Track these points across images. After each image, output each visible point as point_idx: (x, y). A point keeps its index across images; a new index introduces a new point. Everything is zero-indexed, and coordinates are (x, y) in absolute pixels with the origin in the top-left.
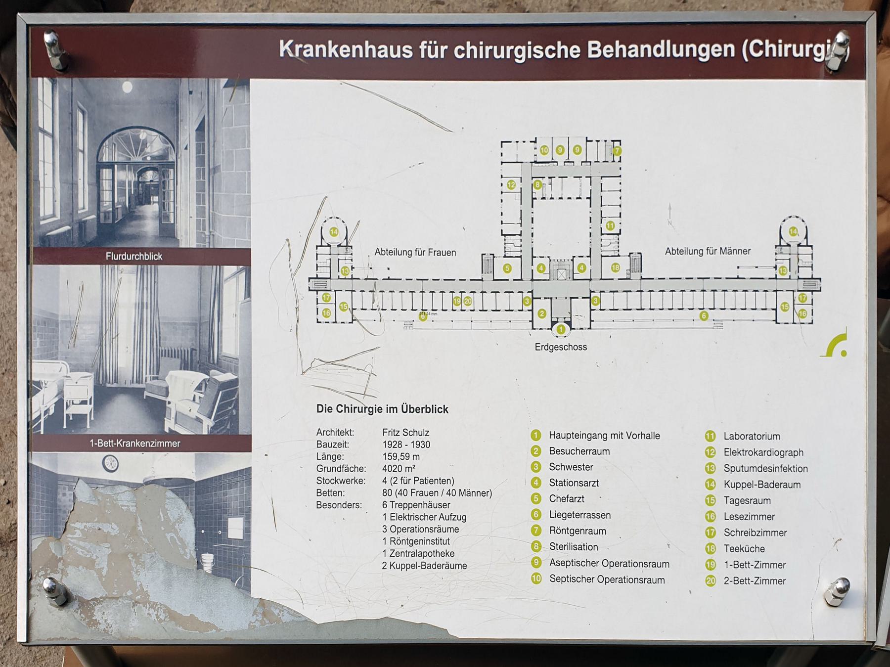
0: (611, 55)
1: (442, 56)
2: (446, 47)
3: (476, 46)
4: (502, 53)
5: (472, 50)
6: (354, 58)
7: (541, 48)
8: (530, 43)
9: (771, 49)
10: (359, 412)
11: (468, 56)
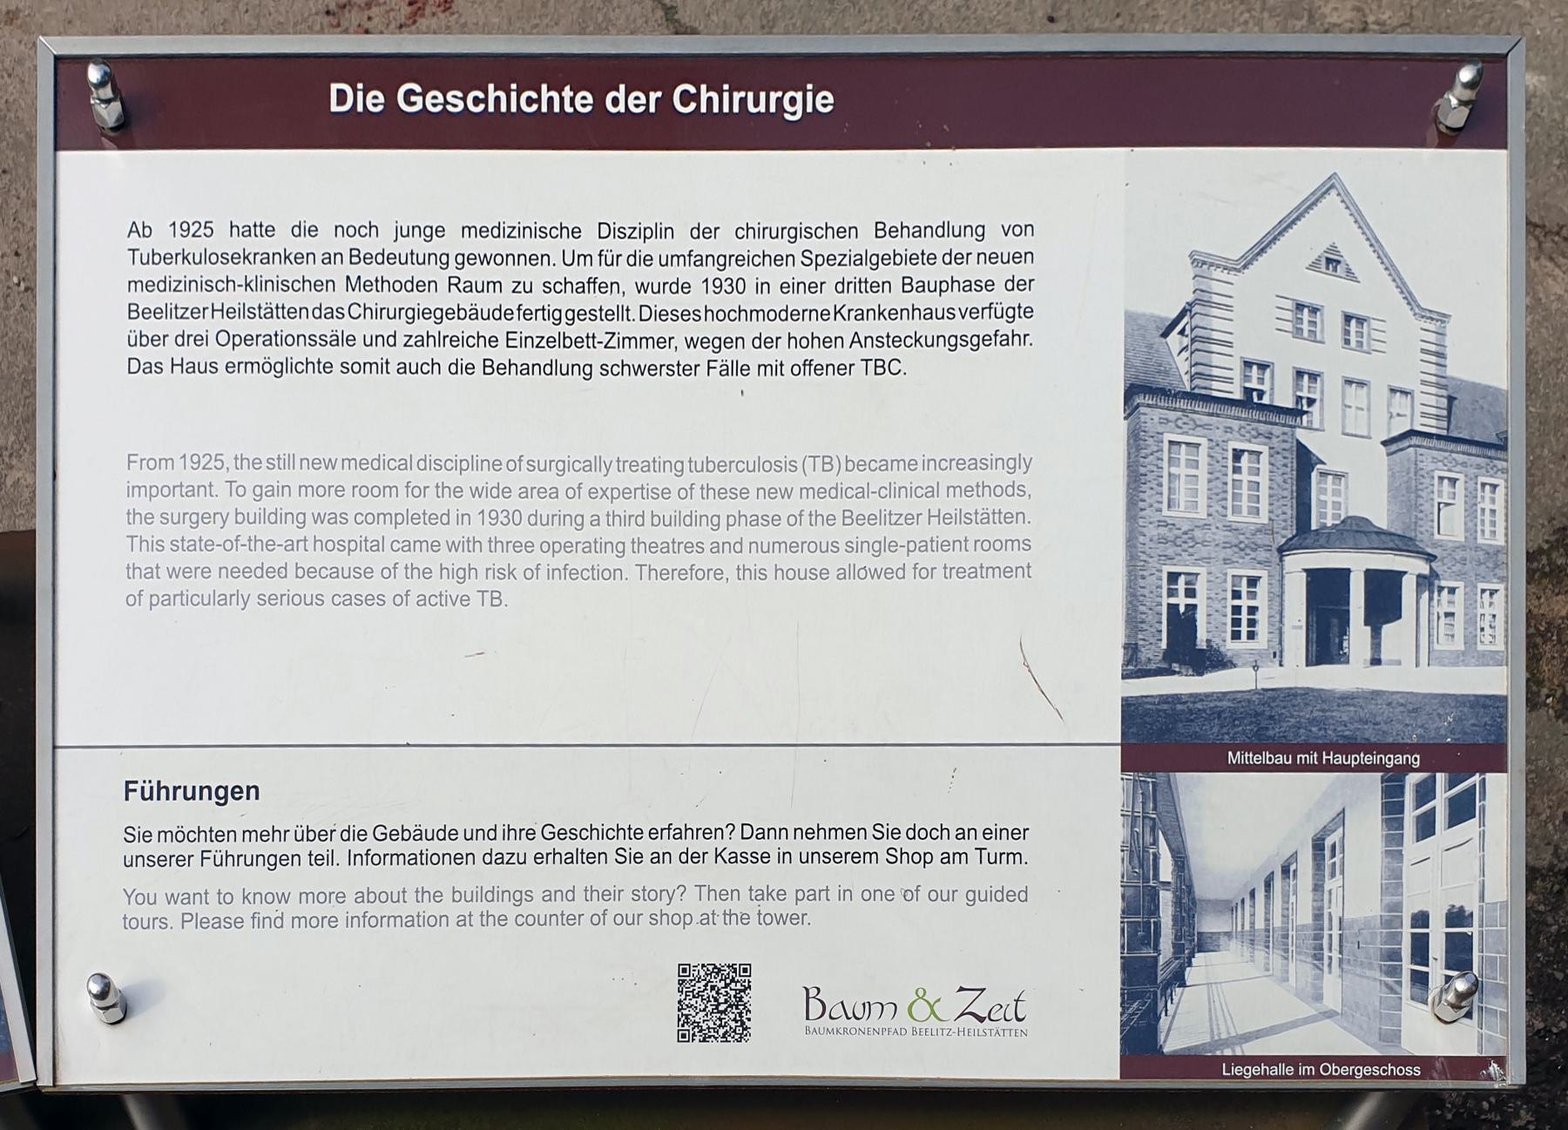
0: (642, 109)
1: (652, 109)
2: (659, 94)
3: (504, 91)
4: (762, 103)
5: (497, 99)
6: (544, 114)
7: (460, 94)
8: (810, 86)
9: (710, 100)
10: (186, 798)
11: (491, 109)
